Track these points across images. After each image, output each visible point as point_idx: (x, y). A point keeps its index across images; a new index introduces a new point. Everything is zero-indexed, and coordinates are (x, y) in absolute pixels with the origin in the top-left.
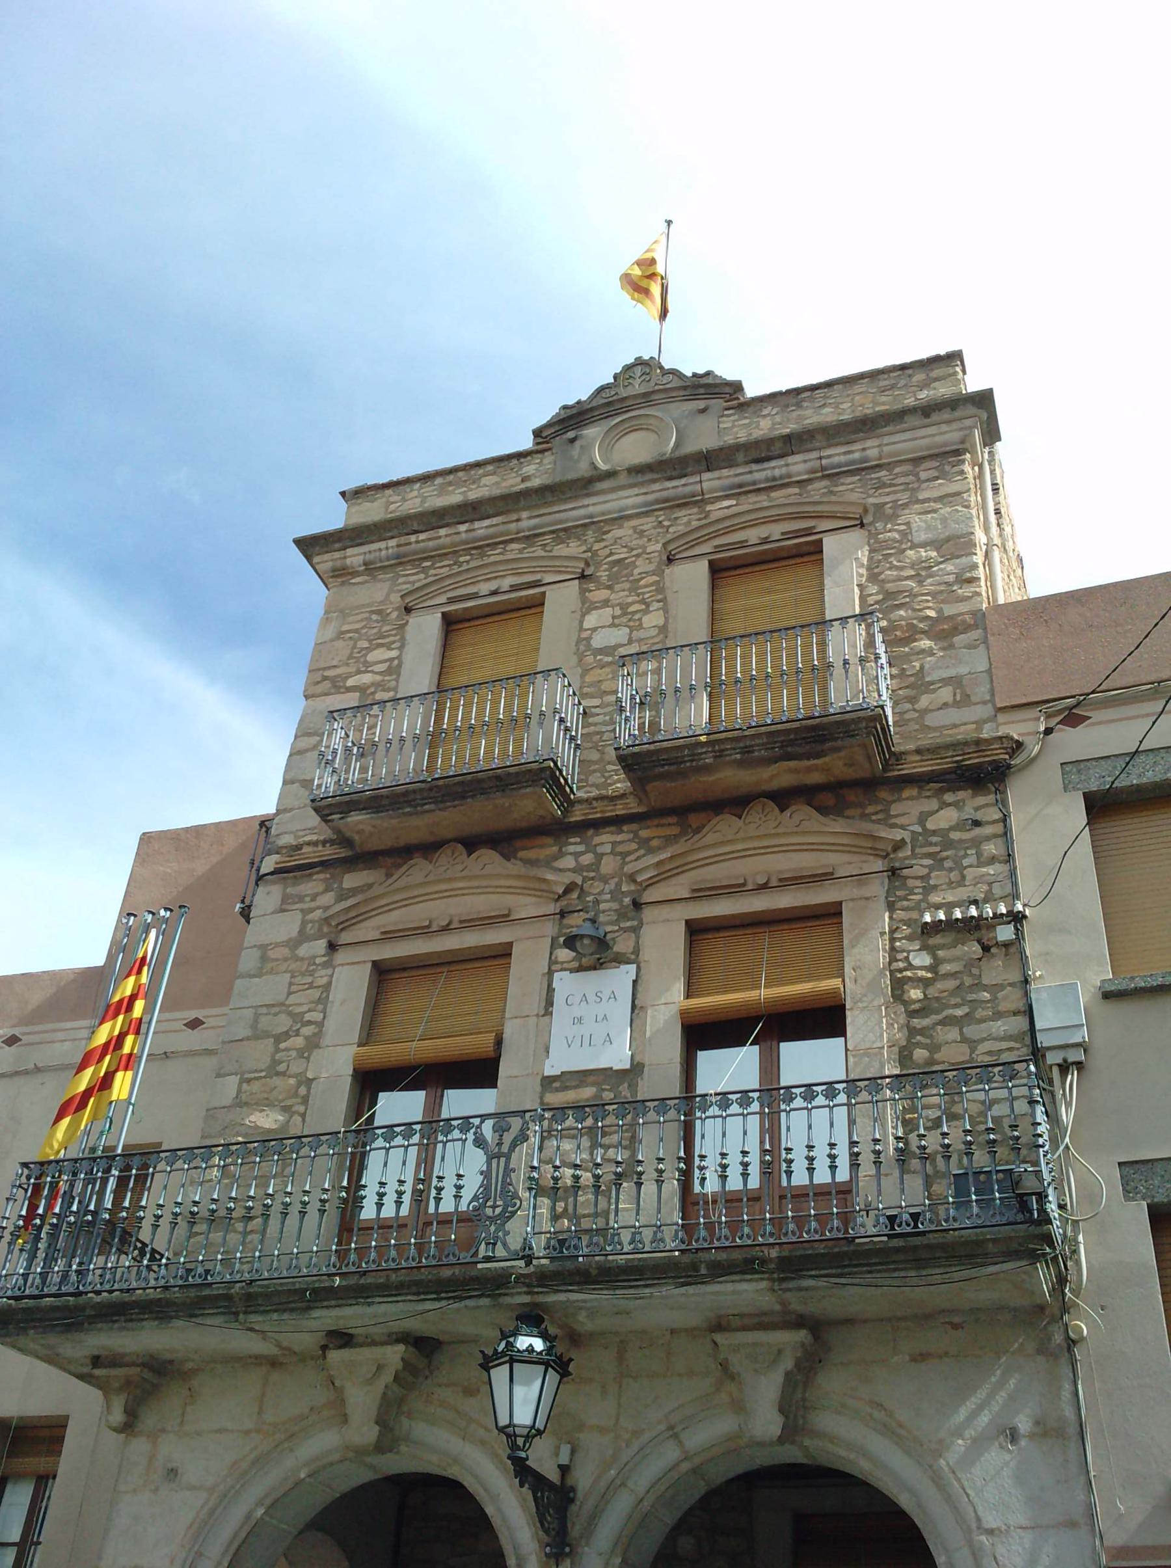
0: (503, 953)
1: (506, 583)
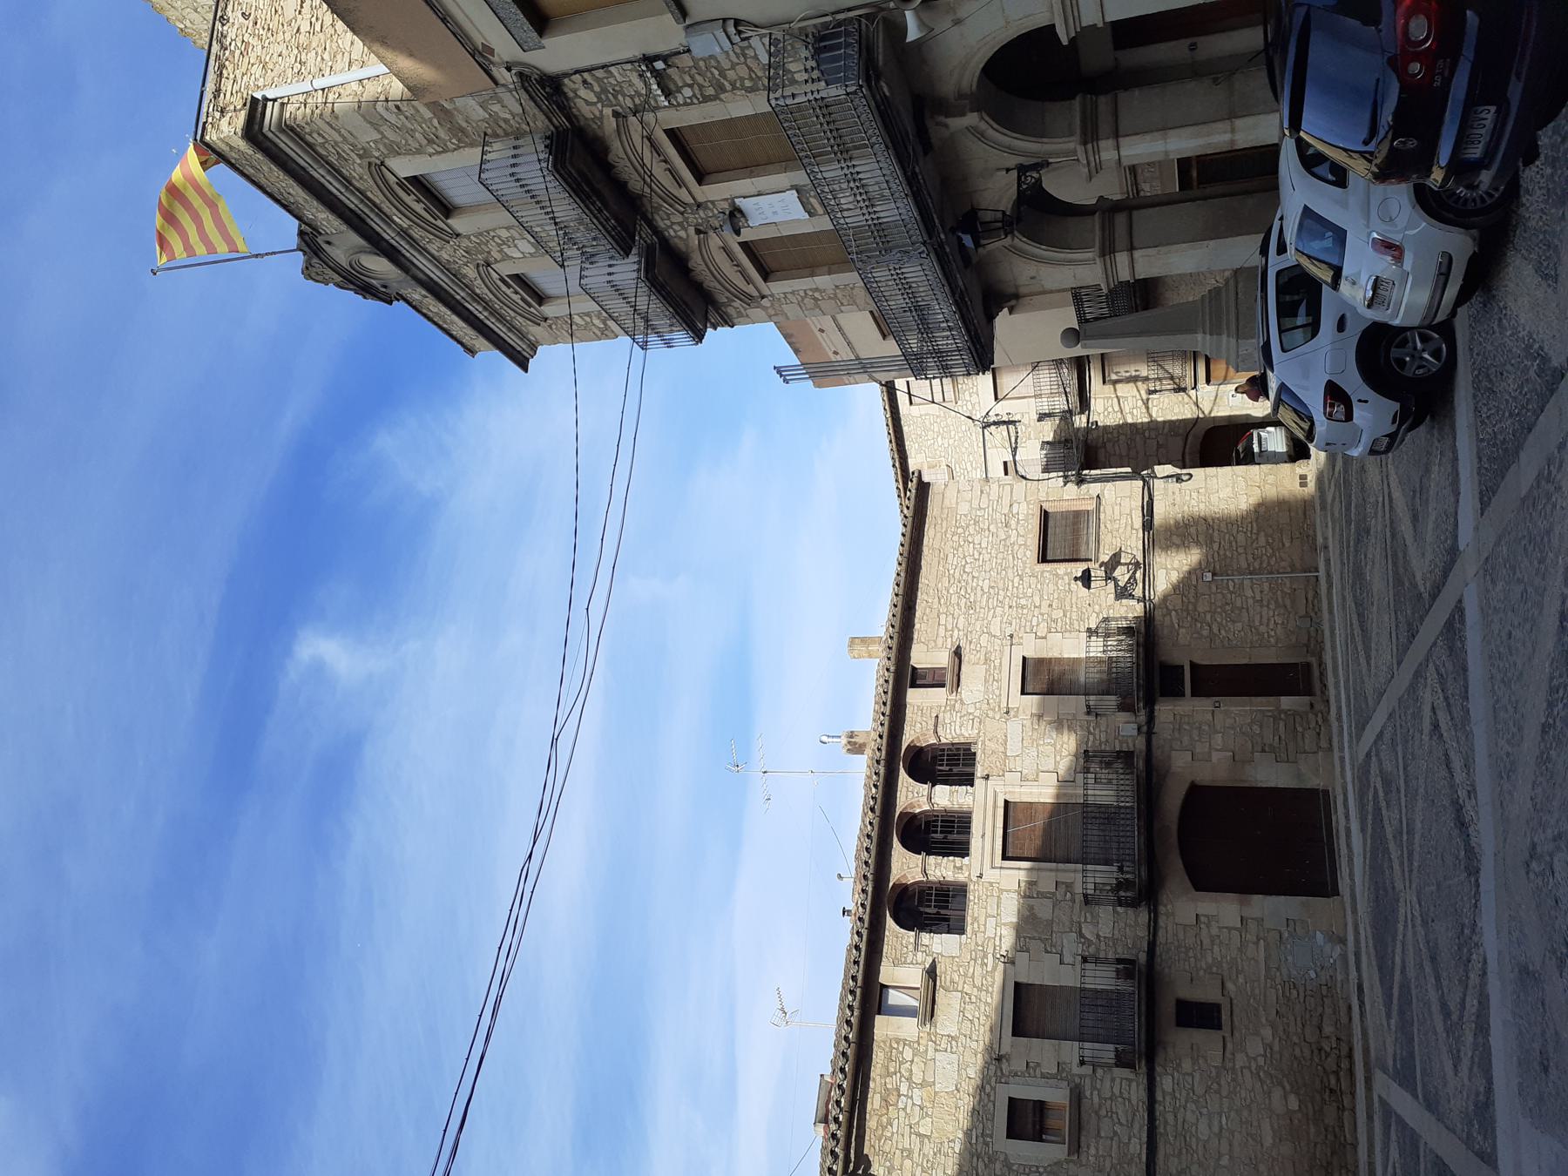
0: (673, 134)
1: (508, 292)
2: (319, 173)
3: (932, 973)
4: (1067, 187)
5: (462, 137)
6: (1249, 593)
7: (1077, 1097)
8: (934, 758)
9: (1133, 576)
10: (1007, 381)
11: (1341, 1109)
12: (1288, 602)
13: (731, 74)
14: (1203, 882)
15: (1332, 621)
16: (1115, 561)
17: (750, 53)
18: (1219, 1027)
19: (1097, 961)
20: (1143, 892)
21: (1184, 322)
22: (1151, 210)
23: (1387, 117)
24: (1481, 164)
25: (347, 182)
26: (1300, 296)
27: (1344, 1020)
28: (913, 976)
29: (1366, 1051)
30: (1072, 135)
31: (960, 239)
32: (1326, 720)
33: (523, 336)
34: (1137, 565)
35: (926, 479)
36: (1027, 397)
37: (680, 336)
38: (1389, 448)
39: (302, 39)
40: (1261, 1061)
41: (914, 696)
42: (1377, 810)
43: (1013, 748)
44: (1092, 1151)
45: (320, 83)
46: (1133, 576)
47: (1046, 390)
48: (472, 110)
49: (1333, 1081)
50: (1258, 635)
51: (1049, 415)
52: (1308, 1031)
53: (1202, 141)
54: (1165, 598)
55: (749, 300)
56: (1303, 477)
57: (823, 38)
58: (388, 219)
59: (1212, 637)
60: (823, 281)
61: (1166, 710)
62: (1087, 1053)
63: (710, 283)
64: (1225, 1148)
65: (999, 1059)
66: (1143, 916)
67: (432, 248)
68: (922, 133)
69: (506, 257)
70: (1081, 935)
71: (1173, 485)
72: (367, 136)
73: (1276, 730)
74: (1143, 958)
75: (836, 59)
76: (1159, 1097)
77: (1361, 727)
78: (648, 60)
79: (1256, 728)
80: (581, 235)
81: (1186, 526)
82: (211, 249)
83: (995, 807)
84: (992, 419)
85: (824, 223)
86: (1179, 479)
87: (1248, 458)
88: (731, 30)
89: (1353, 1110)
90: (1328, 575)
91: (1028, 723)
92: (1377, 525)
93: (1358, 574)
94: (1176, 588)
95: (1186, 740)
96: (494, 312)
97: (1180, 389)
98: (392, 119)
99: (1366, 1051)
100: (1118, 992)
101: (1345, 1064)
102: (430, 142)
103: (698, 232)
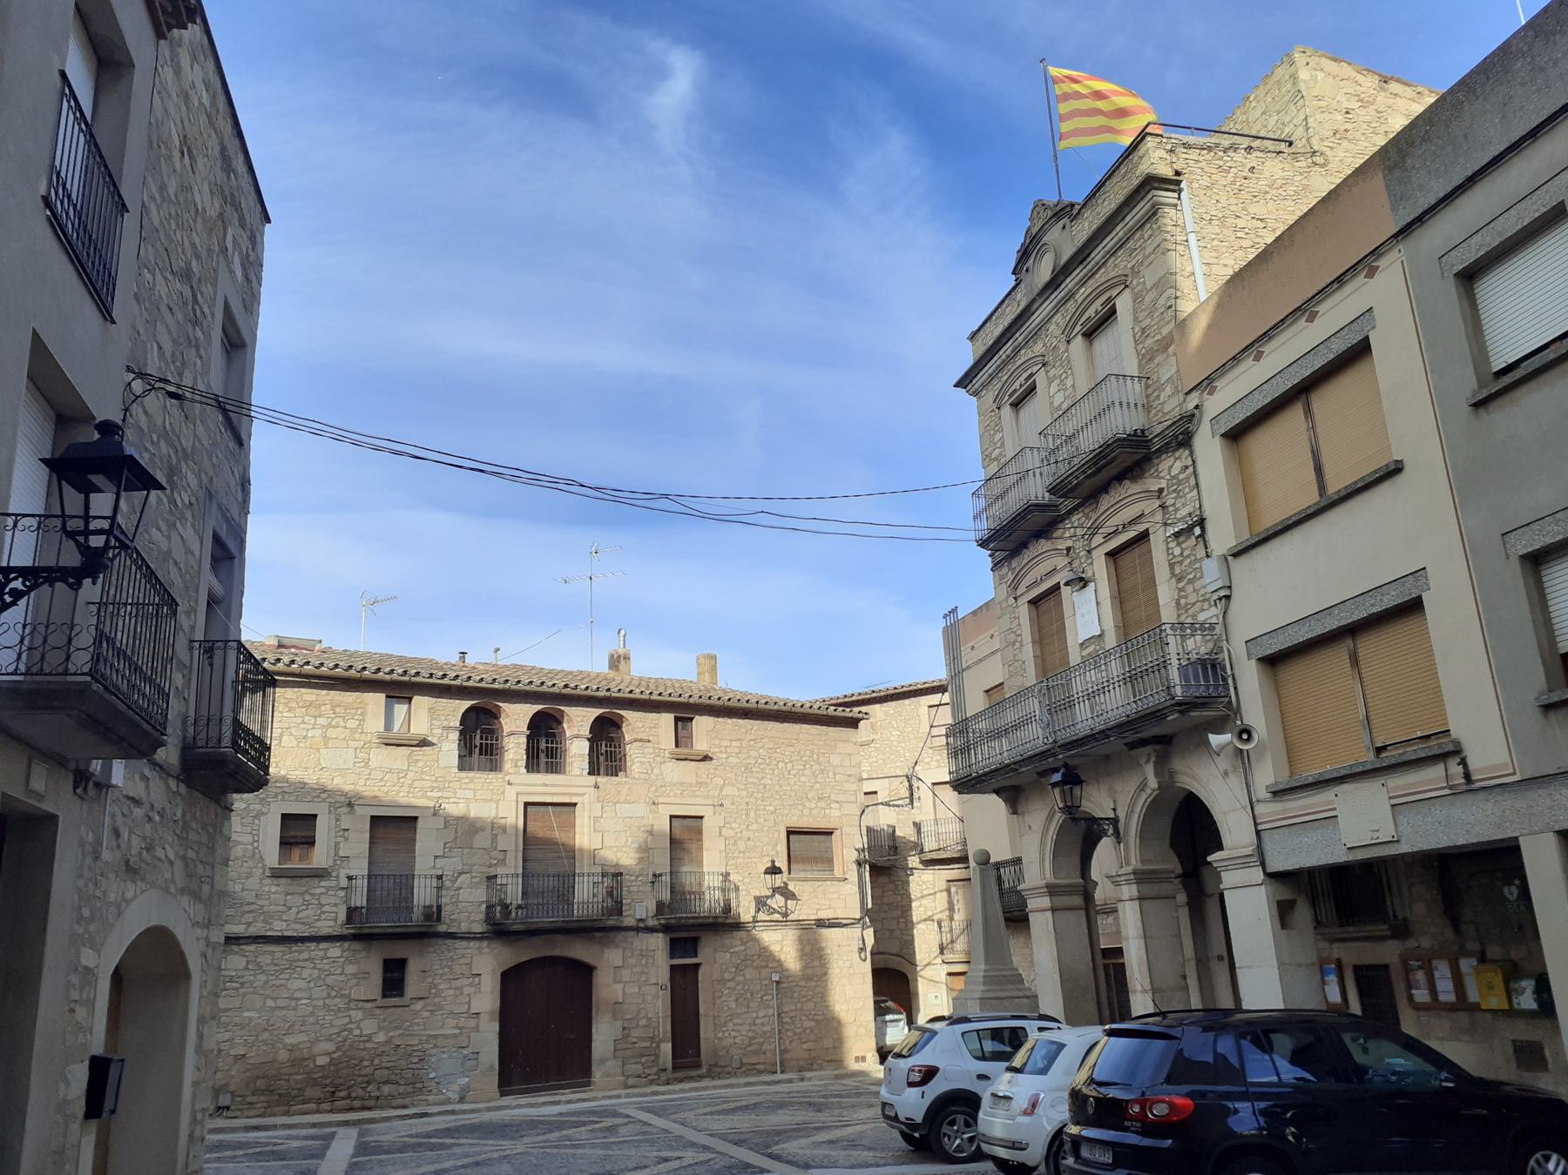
0: (1144, 536)
2: (1119, 231)
3: (424, 743)
4: (1105, 857)
5: (1146, 358)
6: (761, 1014)
7: (320, 874)
8: (612, 739)
9: (775, 912)
10: (949, 795)
11: (319, 1101)
12: (754, 1048)
13: (1190, 589)
14: (510, 979)
15: (738, 1085)
16: (788, 895)
17: (1206, 605)
18: (384, 996)
19: (439, 888)
20: (499, 929)
21: (994, 952)
22: (1085, 925)
23: (1112, 1093)
24: (1077, 1156)
25: (1113, 253)
26: (1005, 1044)
27: (400, 1101)
28: (419, 727)
29: (371, 1121)
30: (1143, 862)
31: (1056, 770)
32: (652, 1082)
33: (984, 386)
34: (786, 915)
35: (861, 724)
36: (939, 817)
37: (984, 526)
38: (886, 1117)
39: (1231, 221)
40: (357, 1032)
41: (667, 719)
42: (584, 1124)
43: (624, 810)
44: (274, 889)
45: (1192, 238)
46: (775, 912)
47: (942, 829)
48: (1166, 371)
49: (342, 1094)
50: (727, 1021)
51: (919, 832)
52: (385, 1072)
53: (1135, 967)
54: (756, 940)
55: (1014, 586)
56: (863, 1059)
57: (1214, 666)
58: (1083, 283)
59: (722, 981)
60: (1028, 652)
61: (659, 942)
62: (359, 882)
63: (1027, 555)
64: (281, 1003)
65: (350, 805)
66: (478, 928)
67: (1058, 318)
68: (1144, 742)
69: (1050, 381)
70: (460, 874)
71: (857, 944)
72: (1149, 277)
73: (643, 1039)
74: (442, 928)
75: (1196, 678)
76: (323, 945)
77: (650, 1110)
78: (1201, 522)
79: (643, 1022)
80: (1063, 454)
81: (821, 958)
82: (1062, 118)
83: (570, 794)
84: (915, 783)
85: (1075, 658)
86: (862, 950)
87: (880, 1011)
88: (1222, 593)
89: (318, 1112)
90: (778, 1082)
91: (645, 822)
92: (823, 1117)
93: (782, 1105)
94: (765, 949)
95: (632, 961)
96: (1005, 363)
97: (942, 950)
98: (1162, 301)
99: (371, 1121)
100: (410, 909)
101: (356, 1104)
102: (1143, 330)
103: (1068, 549)
